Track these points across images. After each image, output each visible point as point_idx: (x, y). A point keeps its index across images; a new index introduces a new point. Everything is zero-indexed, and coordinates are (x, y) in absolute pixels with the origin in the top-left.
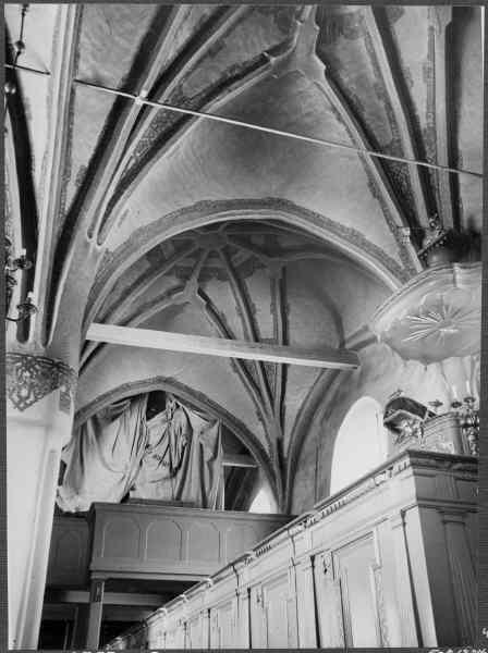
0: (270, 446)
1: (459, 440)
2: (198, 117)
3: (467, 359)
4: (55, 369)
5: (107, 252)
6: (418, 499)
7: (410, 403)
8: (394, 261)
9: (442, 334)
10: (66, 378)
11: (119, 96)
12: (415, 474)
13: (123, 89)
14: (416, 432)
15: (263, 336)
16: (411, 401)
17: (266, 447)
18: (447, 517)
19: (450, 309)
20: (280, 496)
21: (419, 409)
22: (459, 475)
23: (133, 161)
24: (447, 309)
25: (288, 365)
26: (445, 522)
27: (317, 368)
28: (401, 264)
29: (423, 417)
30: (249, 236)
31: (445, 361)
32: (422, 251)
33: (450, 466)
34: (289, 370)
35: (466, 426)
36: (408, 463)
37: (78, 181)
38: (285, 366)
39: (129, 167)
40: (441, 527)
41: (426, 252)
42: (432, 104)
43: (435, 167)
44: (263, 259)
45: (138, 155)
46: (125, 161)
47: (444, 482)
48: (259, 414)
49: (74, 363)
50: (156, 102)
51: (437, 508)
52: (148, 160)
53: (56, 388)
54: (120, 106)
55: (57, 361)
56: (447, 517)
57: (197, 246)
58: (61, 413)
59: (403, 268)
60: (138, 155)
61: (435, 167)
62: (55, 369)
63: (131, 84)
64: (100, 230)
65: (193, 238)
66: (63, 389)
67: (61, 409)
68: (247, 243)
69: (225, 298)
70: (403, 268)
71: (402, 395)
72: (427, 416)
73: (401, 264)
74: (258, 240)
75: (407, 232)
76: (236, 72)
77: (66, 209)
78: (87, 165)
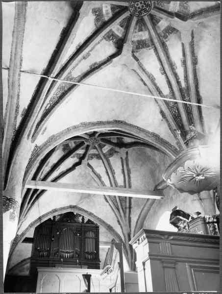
0: (125, 237)
1: (206, 229)
2: (57, 81)
3: (212, 191)
4: (8, 201)
5: (36, 146)
6: (149, 255)
7: (182, 213)
8: (174, 147)
9: (197, 180)
10: (13, 205)
11: (42, 77)
12: (149, 242)
13: (44, 74)
14: (185, 227)
15: (119, 185)
16: (183, 212)
17: (123, 239)
18: (165, 265)
19: (199, 167)
20: (130, 261)
21: (187, 216)
22: (172, 242)
23: (49, 105)
24: (198, 167)
25: (132, 198)
26: (164, 267)
27: (145, 199)
28: (178, 148)
29: (188, 219)
30: (110, 138)
31: (201, 193)
32: (186, 141)
33: (168, 238)
34: (132, 200)
35: (209, 223)
36: (145, 237)
37: (22, 115)
38: (130, 198)
39: (47, 108)
40: (162, 269)
41: (188, 141)
42: (186, 77)
43: (190, 103)
44: (117, 149)
45: (51, 102)
46: (45, 105)
47: (206, 253)
48: (118, 221)
49: (19, 199)
50: (59, 79)
51: (160, 260)
52: (56, 105)
53: (8, 210)
54: (42, 82)
55: (9, 197)
56: (165, 265)
57: (86, 144)
58: (11, 222)
59: (178, 149)
60: (51, 102)
61: (190, 103)
62: (8, 201)
63: (47, 71)
64: (33, 136)
65: (83, 140)
66: (11, 210)
67: (10, 220)
68: (109, 142)
69: (99, 166)
70: (178, 149)
71: (178, 209)
72: (190, 219)
73: (178, 148)
74: (114, 139)
75: (179, 132)
76: (96, 66)
77: (17, 127)
78: (26, 108)
